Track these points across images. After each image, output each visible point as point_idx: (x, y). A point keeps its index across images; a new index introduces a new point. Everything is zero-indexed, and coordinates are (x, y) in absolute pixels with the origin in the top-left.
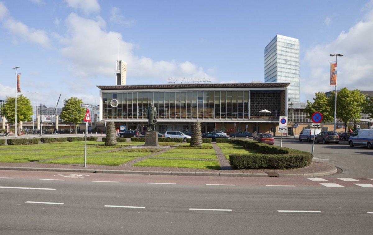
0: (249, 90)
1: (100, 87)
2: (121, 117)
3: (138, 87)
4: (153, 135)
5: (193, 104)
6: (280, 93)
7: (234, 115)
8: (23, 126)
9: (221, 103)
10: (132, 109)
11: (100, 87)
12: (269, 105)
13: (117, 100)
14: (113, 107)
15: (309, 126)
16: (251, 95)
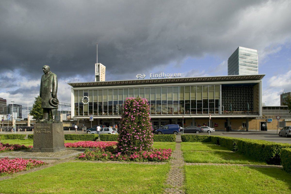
0: (220, 84)
1: (71, 84)
2: (92, 114)
3: (127, 82)
4: (47, 129)
5: (185, 100)
6: (253, 87)
7: (204, 110)
8: (30, 124)
9: (203, 100)
10: (92, 106)
11: (71, 84)
12: (241, 100)
13: (88, 97)
14: (85, 104)
15: (284, 120)
16: (222, 88)
